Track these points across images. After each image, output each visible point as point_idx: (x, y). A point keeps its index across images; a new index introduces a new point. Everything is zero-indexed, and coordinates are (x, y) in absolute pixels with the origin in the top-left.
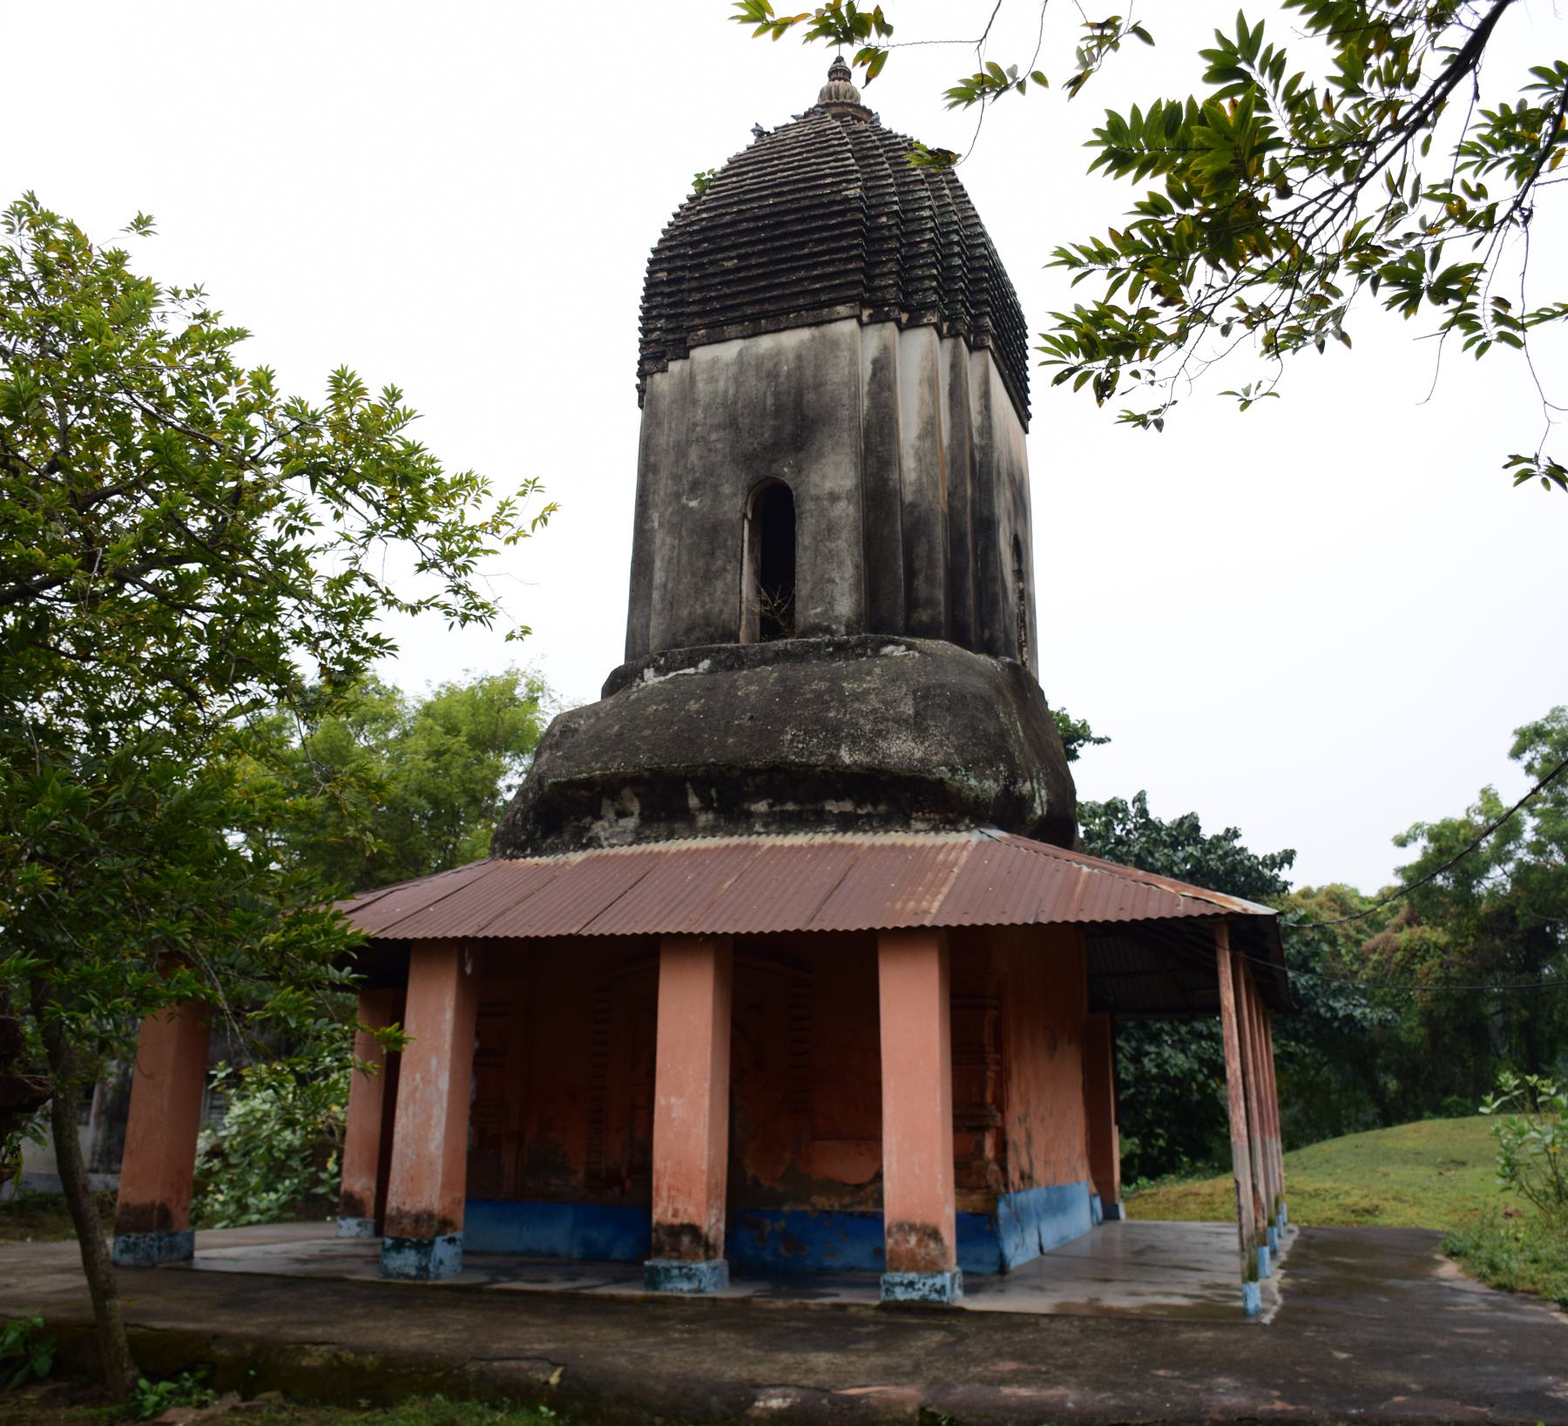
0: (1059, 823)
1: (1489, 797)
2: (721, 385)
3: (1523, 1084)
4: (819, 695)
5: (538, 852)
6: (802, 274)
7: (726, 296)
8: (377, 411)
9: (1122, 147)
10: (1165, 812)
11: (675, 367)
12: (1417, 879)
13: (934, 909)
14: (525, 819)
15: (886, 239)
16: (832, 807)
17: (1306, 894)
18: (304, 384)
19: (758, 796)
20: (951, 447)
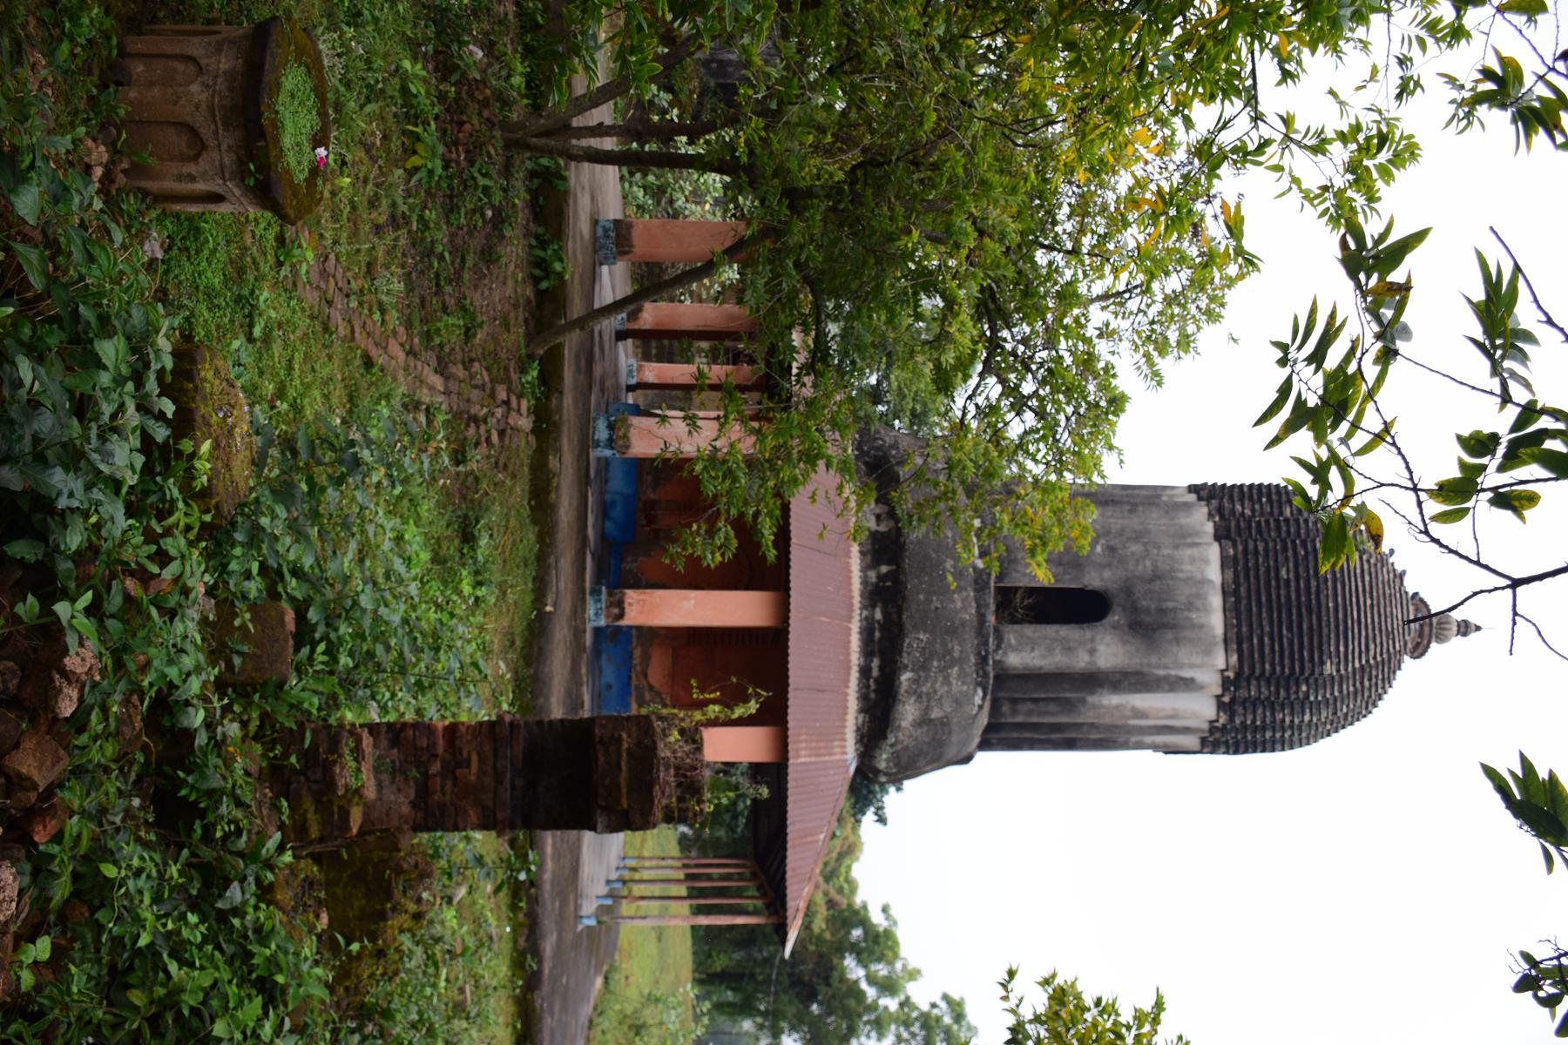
0: (865, 789)
1: (914, 975)
2: (1188, 567)
4: (950, 652)
6: (1267, 629)
7: (1257, 570)
11: (1209, 527)
12: (857, 917)
14: (879, 448)
15: (1288, 690)
16: (876, 663)
19: (885, 614)
20: (1127, 726)
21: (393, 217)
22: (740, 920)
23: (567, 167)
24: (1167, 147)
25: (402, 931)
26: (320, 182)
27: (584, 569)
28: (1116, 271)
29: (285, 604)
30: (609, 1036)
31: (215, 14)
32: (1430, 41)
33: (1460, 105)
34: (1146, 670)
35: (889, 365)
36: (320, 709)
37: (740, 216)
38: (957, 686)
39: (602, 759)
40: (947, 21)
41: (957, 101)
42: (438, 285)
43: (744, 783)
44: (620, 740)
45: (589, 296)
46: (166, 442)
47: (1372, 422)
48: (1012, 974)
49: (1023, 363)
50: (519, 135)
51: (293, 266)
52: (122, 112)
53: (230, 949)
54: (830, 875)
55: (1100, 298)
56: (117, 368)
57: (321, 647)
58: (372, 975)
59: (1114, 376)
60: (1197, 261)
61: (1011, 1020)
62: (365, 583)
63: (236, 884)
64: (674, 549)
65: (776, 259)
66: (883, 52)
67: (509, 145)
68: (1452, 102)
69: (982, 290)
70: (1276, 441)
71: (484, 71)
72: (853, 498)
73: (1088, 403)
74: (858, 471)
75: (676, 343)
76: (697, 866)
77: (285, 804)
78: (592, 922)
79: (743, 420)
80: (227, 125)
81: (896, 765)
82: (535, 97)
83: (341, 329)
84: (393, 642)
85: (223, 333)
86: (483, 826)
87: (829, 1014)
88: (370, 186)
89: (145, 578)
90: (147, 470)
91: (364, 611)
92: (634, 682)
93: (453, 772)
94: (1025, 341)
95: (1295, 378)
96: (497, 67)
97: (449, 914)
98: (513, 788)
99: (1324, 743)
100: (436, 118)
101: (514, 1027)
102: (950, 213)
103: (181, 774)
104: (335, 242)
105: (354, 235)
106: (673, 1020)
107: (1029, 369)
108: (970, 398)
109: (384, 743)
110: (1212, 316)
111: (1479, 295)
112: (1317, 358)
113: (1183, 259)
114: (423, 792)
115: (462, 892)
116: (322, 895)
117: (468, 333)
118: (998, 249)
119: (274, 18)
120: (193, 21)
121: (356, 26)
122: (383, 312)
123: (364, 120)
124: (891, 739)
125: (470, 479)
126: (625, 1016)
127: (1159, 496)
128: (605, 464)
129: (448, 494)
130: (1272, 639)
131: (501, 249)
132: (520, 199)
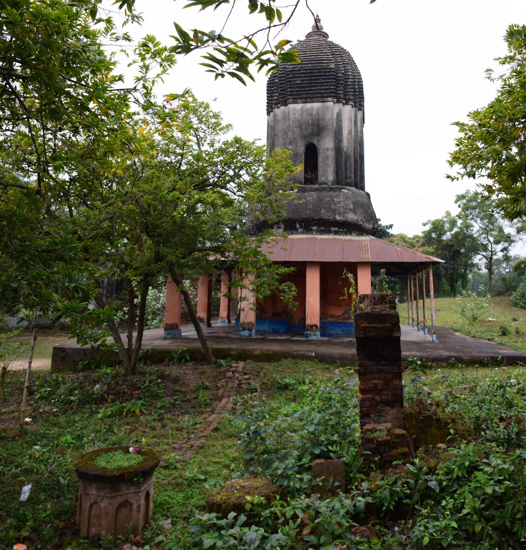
0: (380, 233)
1: (448, 214)
2: (297, 115)
4: (328, 201)
11: (282, 108)
12: (427, 235)
14: (253, 228)
16: (333, 229)
19: (314, 225)
21: (159, 420)
22: (431, 279)
23: (143, 350)
24: (145, 122)
25: (444, 412)
26: (143, 450)
27: (298, 340)
28: (189, 141)
29: (313, 464)
30: (478, 330)
31: (74, 497)
32: (113, 31)
33: (134, 20)
34: (334, 130)
35: (222, 224)
36: (355, 448)
37: (164, 283)
38: (341, 199)
39: (372, 334)
40: (96, 200)
41: (125, 197)
42: (187, 401)
43: (379, 278)
44: (364, 327)
45: (193, 340)
46: (246, 516)
47: (244, 43)
48: (448, 177)
49: (222, 174)
50: (130, 369)
51: (177, 462)
52: (111, 538)
53: (456, 487)
54: (412, 246)
55: (199, 147)
56: (215, 538)
57: (330, 448)
58: (462, 425)
59: (227, 141)
60: (188, 111)
61: (466, 177)
62: (304, 429)
63: (429, 484)
64: (291, 307)
65: (181, 266)
66: (105, 225)
67: (133, 373)
68: (132, 23)
69: (195, 189)
70: (251, 77)
71: (104, 384)
72: (271, 238)
73: (237, 151)
74: (262, 236)
75: (213, 304)
76: (411, 296)
77: (395, 462)
78: (435, 336)
79: (242, 279)
80: (118, 491)
81: (371, 221)
82: (116, 363)
83: (202, 441)
84: (327, 418)
85: (203, 492)
86: (400, 378)
87: (465, 245)
88: (147, 430)
89: (303, 525)
90: (258, 524)
91: (315, 430)
92: (341, 321)
93: (379, 390)
94: (214, 174)
95: (228, 71)
96: (103, 379)
97: (435, 394)
98: (384, 365)
99: (359, 67)
100: (121, 403)
101: (478, 367)
102: (166, 201)
103: (384, 508)
104: (168, 444)
105: (165, 436)
106: (470, 305)
107: (224, 172)
108: (235, 194)
109: (368, 420)
110: (207, 107)
111: (200, 6)
112: (221, 63)
113: (186, 117)
114: (387, 403)
115: (426, 388)
116: (431, 446)
117: (206, 388)
118: (180, 183)
119: (76, 470)
120: (76, 507)
121: (83, 437)
122: (196, 424)
123: (120, 433)
124: (361, 223)
125: (263, 386)
126: (470, 323)
127: (271, 126)
128: (258, 332)
129: (269, 396)
130: (322, 86)
131: (174, 376)
132: (154, 368)
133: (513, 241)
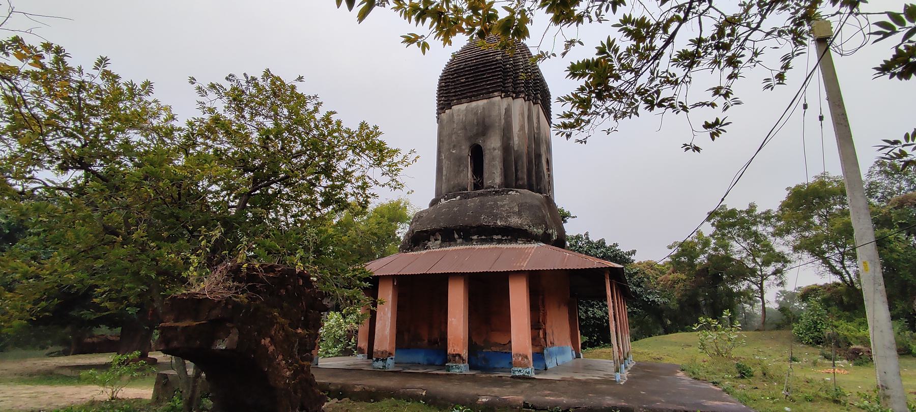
0: (560, 242)
3: (707, 321)
5: (412, 251)
8: (372, 132)
9: (575, 71)
10: (594, 238)
13: (525, 266)
16: (495, 237)
17: (640, 263)
18: (352, 124)
124: (527, 227)
133: (790, 262)
